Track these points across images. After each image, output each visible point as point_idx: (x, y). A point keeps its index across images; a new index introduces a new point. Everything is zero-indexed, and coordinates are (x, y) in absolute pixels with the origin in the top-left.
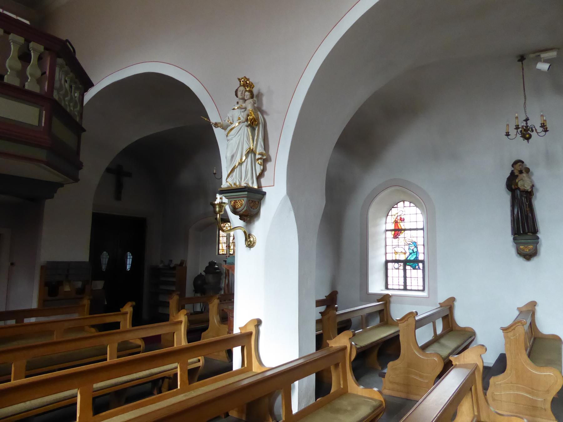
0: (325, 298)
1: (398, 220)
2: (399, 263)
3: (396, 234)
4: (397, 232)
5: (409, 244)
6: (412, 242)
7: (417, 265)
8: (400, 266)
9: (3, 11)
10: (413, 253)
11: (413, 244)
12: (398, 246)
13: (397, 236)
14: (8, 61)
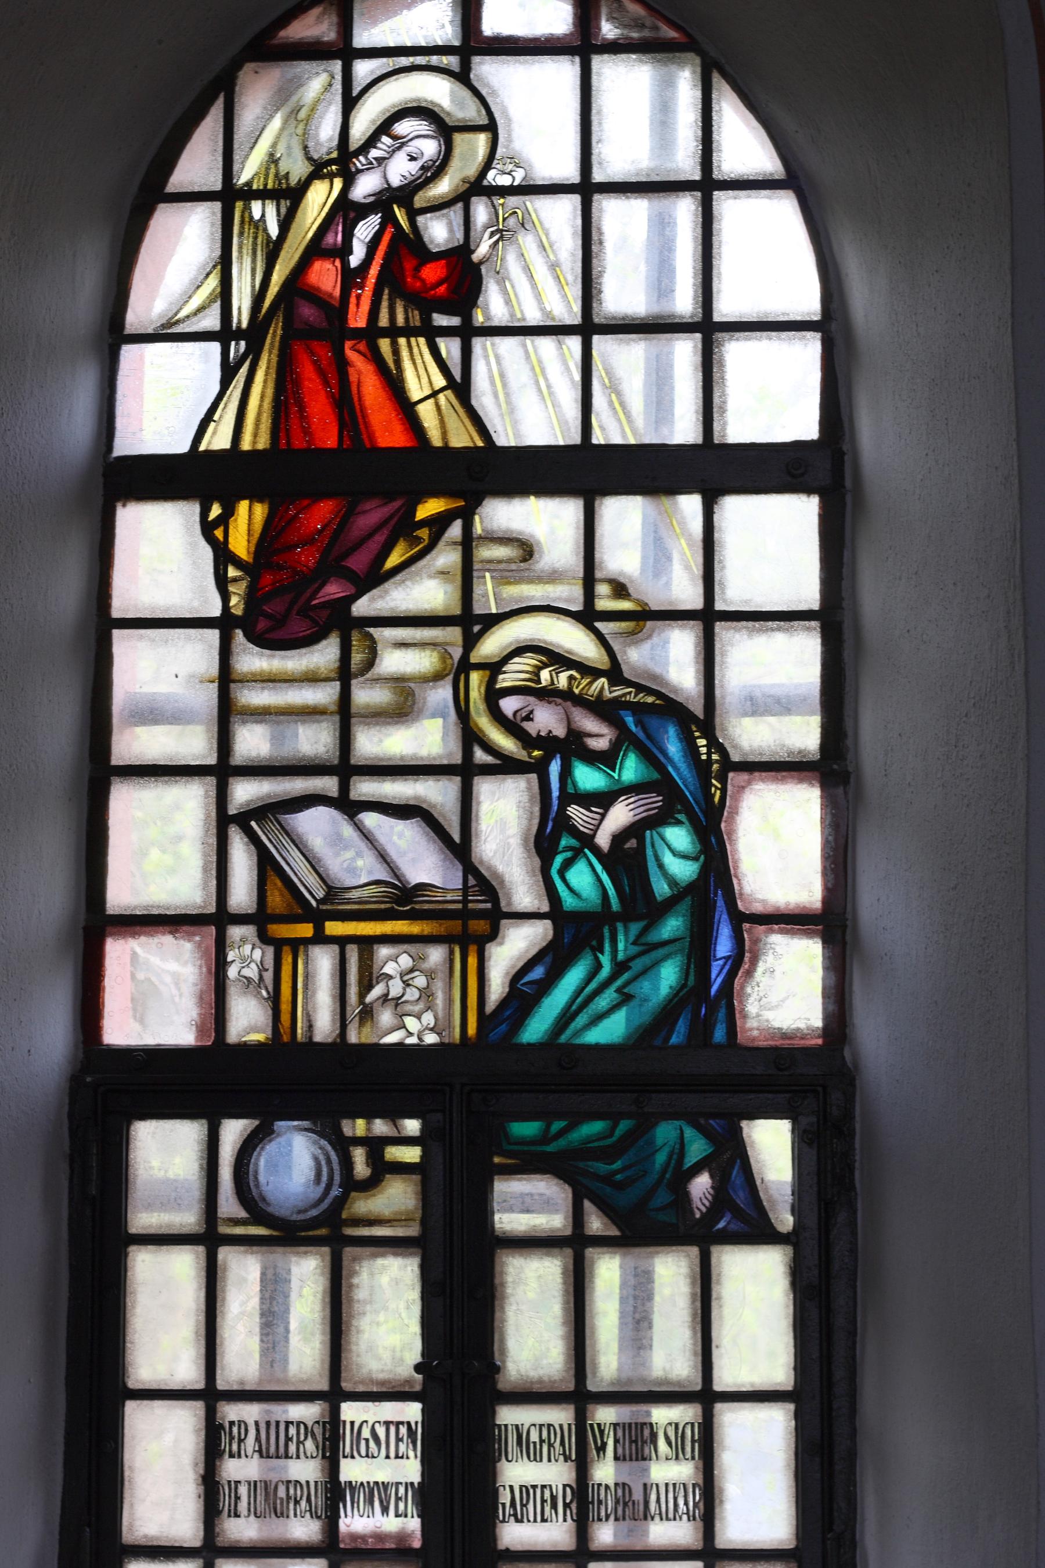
0: (534, 735)
1: (351, 278)
2: (493, 166)
3: (308, 558)
4: (325, 510)
5: (548, 744)
6: (600, 708)
7: (697, 1148)
8: (361, 1168)
9: (276, 740)
10: (627, 916)
11: (624, 740)
12: (329, 785)
13: (333, 590)
14: (737, 980)
